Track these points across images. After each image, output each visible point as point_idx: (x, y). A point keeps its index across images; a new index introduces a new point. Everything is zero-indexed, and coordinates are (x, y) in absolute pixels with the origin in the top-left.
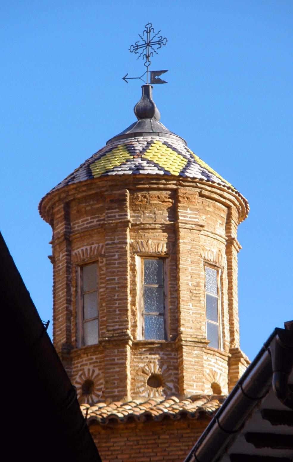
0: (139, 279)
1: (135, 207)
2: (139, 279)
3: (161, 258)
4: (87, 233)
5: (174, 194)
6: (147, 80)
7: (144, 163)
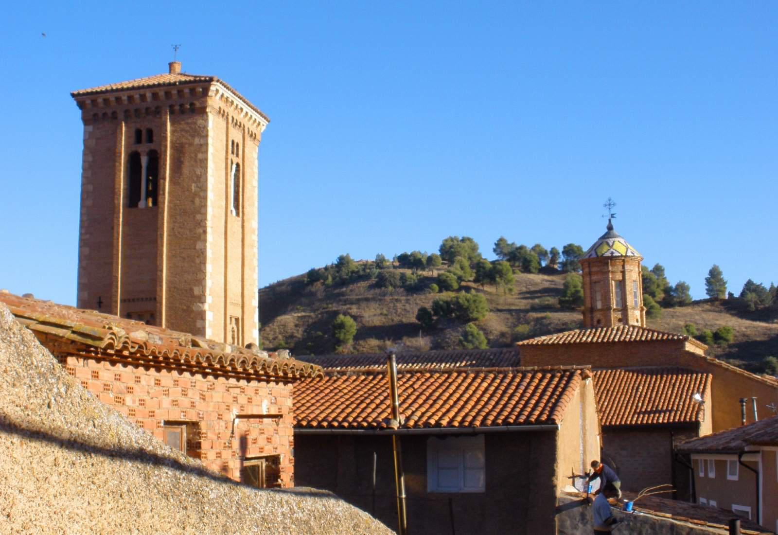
0: (614, 288)
1: (611, 265)
2: (614, 288)
3: (620, 281)
4: (597, 273)
5: (624, 261)
6: (609, 217)
7: (614, 251)
